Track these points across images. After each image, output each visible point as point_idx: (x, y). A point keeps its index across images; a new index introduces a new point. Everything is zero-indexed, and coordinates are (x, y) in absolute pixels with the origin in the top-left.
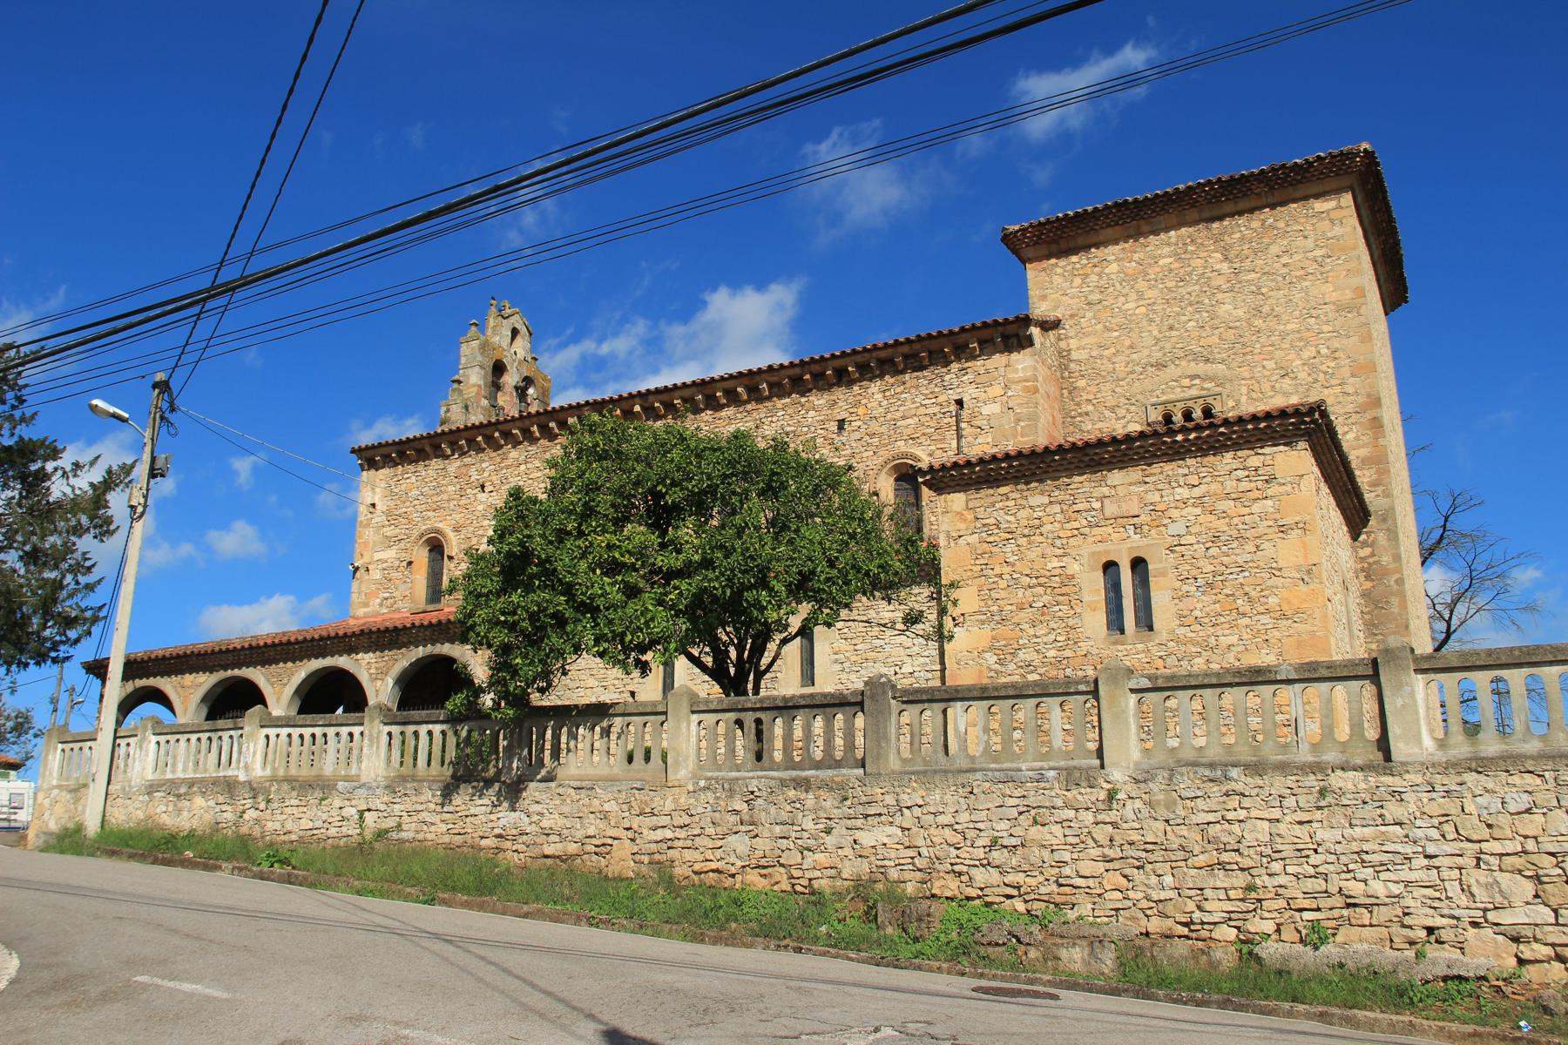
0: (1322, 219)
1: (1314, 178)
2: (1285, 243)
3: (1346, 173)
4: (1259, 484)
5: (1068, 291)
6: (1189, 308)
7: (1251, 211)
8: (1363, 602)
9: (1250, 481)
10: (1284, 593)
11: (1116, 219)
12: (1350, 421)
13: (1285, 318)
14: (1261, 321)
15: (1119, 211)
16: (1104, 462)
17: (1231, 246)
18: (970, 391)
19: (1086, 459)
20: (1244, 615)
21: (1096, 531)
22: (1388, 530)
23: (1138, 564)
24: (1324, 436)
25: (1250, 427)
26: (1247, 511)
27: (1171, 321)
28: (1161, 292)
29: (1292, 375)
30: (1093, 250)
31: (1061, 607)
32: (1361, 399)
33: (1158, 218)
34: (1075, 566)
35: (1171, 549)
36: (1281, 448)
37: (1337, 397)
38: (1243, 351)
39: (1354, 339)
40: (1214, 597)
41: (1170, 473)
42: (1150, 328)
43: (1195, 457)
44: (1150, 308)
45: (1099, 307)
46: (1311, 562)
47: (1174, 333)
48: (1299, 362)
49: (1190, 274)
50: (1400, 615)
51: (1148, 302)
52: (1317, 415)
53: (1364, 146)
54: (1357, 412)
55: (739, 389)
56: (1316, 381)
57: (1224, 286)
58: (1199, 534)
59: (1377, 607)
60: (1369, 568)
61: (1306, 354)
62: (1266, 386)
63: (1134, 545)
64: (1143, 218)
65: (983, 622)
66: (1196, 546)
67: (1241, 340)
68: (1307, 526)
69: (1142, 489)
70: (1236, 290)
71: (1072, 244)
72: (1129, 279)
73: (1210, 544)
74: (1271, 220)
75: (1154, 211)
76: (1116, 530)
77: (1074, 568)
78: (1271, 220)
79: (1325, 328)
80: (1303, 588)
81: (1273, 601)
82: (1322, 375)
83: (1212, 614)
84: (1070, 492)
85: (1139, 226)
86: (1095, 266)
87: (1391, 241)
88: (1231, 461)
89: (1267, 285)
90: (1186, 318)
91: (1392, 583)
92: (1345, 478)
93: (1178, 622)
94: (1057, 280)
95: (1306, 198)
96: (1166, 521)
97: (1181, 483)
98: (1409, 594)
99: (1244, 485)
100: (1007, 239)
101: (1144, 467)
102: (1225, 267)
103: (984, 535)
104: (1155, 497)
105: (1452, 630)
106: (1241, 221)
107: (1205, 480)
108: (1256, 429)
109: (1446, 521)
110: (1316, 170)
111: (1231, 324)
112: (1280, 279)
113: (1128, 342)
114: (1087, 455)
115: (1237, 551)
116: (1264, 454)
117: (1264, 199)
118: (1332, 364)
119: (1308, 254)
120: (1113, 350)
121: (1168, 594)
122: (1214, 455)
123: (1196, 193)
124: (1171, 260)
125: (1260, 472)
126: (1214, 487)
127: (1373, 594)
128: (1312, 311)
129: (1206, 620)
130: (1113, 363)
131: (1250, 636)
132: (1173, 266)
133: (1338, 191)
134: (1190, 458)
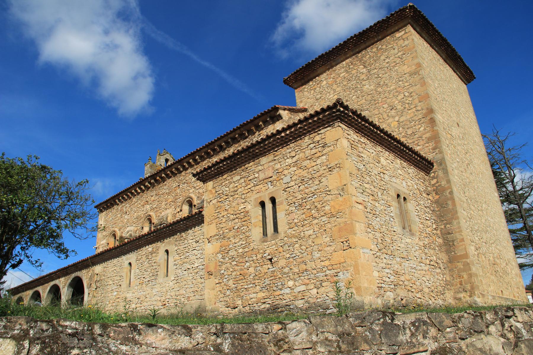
0: (400, 40)
2: (386, 54)
3: (405, 18)
4: (320, 149)
6: (353, 91)
9: (316, 148)
10: (332, 203)
13: (389, 84)
16: (258, 154)
19: (250, 154)
21: (257, 187)
22: (443, 169)
23: (273, 200)
25: (310, 121)
26: (315, 163)
27: (346, 98)
28: (342, 87)
30: (317, 78)
31: (244, 227)
32: (424, 111)
34: (249, 206)
38: (375, 103)
39: (418, 86)
41: (284, 153)
45: (320, 100)
46: (343, 184)
48: (397, 102)
49: (352, 77)
51: (338, 93)
55: (190, 161)
56: (405, 108)
59: (442, 207)
60: (436, 189)
61: (399, 98)
62: (385, 116)
63: (271, 191)
65: (217, 239)
67: (373, 98)
71: (309, 78)
72: (330, 86)
73: (300, 184)
74: (380, 46)
76: (264, 186)
77: (249, 207)
78: (380, 46)
79: (406, 84)
80: (340, 199)
81: (327, 208)
82: (407, 105)
83: (302, 220)
84: (247, 171)
85: (331, 63)
86: (318, 84)
90: (352, 95)
91: (448, 194)
93: (288, 227)
94: (306, 93)
95: (393, 33)
96: (282, 177)
97: (288, 157)
98: (456, 199)
99: (314, 151)
100: (286, 82)
103: (218, 199)
104: (278, 166)
106: (369, 50)
111: (369, 93)
112: (386, 69)
114: (250, 152)
115: (311, 185)
116: (321, 134)
118: (411, 99)
119: (396, 56)
121: (284, 213)
123: (348, 44)
124: (344, 74)
125: (320, 143)
126: (302, 155)
127: (439, 201)
128: (400, 79)
129: (299, 224)
131: (318, 229)
132: (345, 76)
133: (405, 26)
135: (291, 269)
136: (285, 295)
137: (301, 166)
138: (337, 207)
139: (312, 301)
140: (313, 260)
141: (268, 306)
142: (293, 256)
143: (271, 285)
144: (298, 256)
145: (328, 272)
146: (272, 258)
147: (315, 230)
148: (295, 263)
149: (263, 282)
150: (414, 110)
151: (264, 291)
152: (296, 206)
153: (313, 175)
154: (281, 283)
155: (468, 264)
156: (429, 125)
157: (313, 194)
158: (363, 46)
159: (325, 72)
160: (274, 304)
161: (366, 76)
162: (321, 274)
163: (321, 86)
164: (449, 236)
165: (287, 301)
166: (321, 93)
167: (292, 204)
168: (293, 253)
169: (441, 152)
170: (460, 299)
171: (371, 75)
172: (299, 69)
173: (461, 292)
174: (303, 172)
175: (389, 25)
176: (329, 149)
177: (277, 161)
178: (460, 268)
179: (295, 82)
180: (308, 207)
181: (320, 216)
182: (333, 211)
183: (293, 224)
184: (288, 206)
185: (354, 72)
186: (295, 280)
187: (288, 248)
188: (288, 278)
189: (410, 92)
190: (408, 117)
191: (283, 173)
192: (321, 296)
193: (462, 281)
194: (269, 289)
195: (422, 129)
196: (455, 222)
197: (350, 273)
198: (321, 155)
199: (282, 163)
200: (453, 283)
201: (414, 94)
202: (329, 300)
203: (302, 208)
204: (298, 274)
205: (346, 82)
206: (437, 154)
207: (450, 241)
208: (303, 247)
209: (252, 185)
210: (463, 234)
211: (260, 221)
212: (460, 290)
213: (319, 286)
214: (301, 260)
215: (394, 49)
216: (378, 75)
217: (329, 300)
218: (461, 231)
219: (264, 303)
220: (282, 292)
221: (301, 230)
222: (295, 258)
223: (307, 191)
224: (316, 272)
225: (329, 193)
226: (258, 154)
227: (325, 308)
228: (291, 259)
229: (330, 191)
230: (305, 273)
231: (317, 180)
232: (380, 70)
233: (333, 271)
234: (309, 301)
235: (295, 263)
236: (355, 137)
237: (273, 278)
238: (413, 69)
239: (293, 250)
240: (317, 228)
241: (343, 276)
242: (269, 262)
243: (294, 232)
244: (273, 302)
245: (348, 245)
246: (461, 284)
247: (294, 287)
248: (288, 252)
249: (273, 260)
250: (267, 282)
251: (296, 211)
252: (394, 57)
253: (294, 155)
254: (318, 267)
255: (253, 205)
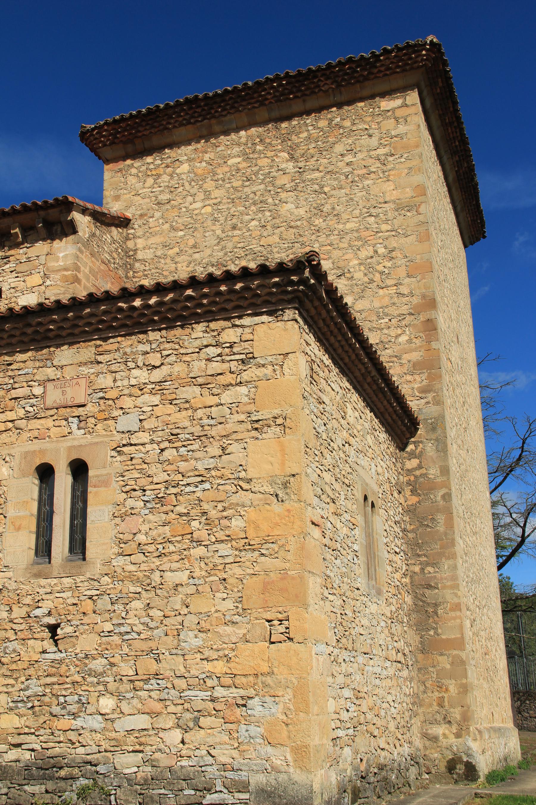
0: (388, 118)
1: (381, 75)
2: (350, 141)
3: (412, 68)
5: (140, 192)
6: (253, 208)
7: (319, 110)
8: (407, 518)
9: (223, 361)
10: (252, 514)
11: (187, 117)
12: (403, 323)
13: (345, 216)
14: (321, 220)
15: (190, 108)
16: (51, 335)
17: (297, 145)
18: (10, 281)
19: (29, 331)
20: (199, 542)
21: (35, 424)
22: (437, 440)
24: (325, 306)
25: (223, 288)
26: (215, 400)
27: (234, 221)
28: (228, 192)
29: (347, 275)
32: (415, 300)
33: (228, 117)
35: (118, 450)
36: (265, 318)
37: (391, 298)
39: (412, 239)
40: (164, 516)
41: (128, 350)
42: (214, 228)
43: (160, 330)
44: (215, 207)
45: (168, 206)
47: (237, 232)
48: (356, 262)
49: (256, 174)
50: (446, 534)
51: (215, 201)
52: (307, 273)
53: (429, 38)
54: (411, 314)
56: (372, 281)
57: (288, 186)
58: (154, 431)
59: (422, 525)
60: (415, 481)
61: (364, 254)
63: (76, 443)
64: (214, 117)
66: (149, 447)
67: (301, 239)
68: (288, 423)
69: (92, 371)
70: (299, 189)
73: (166, 444)
74: (338, 119)
75: (224, 110)
76: (57, 423)
78: (338, 119)
79: (384, 227)
80: (277, 507)
81: (237, 523)
82: (377, 275)
83: (160, 540)
84: (10, 373)
86: (167, 166)
87: (466, 165)
88: (201, 335)
89: (329, 183)
90: (249, 217)
91: (439, 498)
92: (374, 373)
93: (116, 550)
94: (132, 180)
95: (372, 97)
96: (115, 413)
97: (140, 364)
99: (215, 367)
100: (84, 136)
101: (99, 342)
102: (290, 166)
104: (106, 381)
105: (526, 535)
107: (168, 360)
108: (231, 291)
109: (524, 443)
110: (382, 65)
111: (292, 224)
112: (342, 177)
113: (191, 242)
114: (30, 325)
115: (198, 455)
116: (242, 326)
117: (332, 98)
118: (389, 264)
119: (372, 153)
120: (176, 250)
121: (109, 510)
122: (182, 326)
123: (265, 90)
125: (235, 350)
126: (179, 369)
127: (419, 510)
128: (372, 210)
129: (151, 548)
130: (176, 263)
131: (204, 573)
132: (240, 166)
133: (404, 89)
134: (153, 330)
135: (112, 665)
136: (86, 734)
137: (174, 396)
138: (265, 527)
139: (164, 761)
140: (180, 652)
141: (27, 755)
142: (123, 629)
143: (46, 699)
144: (139, 634)
145: (219, 692)
146: (57, 626)
147: (195, 575)
148: (126, 650)
149: (23, 686)
150: (392, 291)
151: (23, 711)
152: (146, 498)
153: (206, 428)
154: (76, 698)
155: (463, 663)
156: (421, 335)
157: (200, 479)
158: (297, 106)
159: (188, 142)
160: (49, 753)
161: (293, 181)
162: (198, 693)
163: (173, 172)
164: (427, 592)
165: (88, 750)
166: (172, 190)
167: (135, 490)
168: (123, 621)
169: (438, 402)
170: (435, 739)
171: (304, 181)
172: (128, 115)
173: (438, 723)
174: (178, 415)
175: (370, 73)
176: (261, 372)
177: (102, 368)
178: (443, 669)
179: (110, 144)
180: (181, 509)
181: (214, 539)
182: (251, 534)
183: (134, 545)
184: (124, 496)
185: (264, 162)
186: (120, 697)
187: (110, 607)
188: (101, 688)
189: (390, 247)
190: (377, 304)
191: (119, 403)
192: (191, 753)
193: (443, 697)
194: (37, 709)
195: (403, 339)
196: (446, 564)
197: (281, 706)
198: (234, 382)
199: (118, 376)
200: (423, 700)
201: (399, 255)
202: (215, 767)
203: (165, 508)
204: (131, 681)
205: (240, 183)
206: (428, 403)
207: (428, 604)
208: (156, 613)
209: (21, 413)
210: (459, 593)
211: (32, 515)
212: (439, 717)
213: (191, 724)
214: (145, 646)
215: (370, 136)
216: (322, 187)
217: (215, 767)
218: (456, 587)
219: (18, 745)
220: (78, 723)
221: (153, 566)
222: (126, 637)
223: (183, 466)
224: (185, 686)
225: (245, 486)
226: (51, 335)
227: (200, 787)
228: (116, 639)
229: (249, 481)
230: (153, 681)
231: (216, 444)
232: (328, 177)
233: (233, 690)
234: (157, 760)
235: (126, 650)
236: (317, 351)
237: (54, 679)
238: (407, 195)
239: (123, 614)
240: (201, 569)
241: (261, 708)
242: (47, 634)
243: (133, 568)
244: (45, 746)
245: (284, 630)
246: (441, 705)
247: (116, 716)
248: (107, 616)
249: (59, 631)
250: (35, 688)
251: (147, 511)
252: (366, 154)
253: (157, 364)
254: (194, 672)
255: (16, 469)
